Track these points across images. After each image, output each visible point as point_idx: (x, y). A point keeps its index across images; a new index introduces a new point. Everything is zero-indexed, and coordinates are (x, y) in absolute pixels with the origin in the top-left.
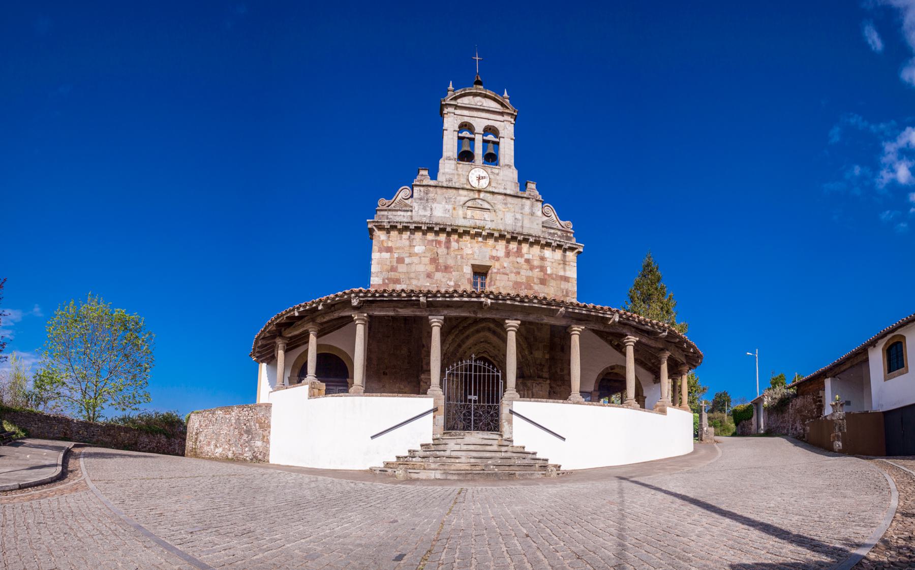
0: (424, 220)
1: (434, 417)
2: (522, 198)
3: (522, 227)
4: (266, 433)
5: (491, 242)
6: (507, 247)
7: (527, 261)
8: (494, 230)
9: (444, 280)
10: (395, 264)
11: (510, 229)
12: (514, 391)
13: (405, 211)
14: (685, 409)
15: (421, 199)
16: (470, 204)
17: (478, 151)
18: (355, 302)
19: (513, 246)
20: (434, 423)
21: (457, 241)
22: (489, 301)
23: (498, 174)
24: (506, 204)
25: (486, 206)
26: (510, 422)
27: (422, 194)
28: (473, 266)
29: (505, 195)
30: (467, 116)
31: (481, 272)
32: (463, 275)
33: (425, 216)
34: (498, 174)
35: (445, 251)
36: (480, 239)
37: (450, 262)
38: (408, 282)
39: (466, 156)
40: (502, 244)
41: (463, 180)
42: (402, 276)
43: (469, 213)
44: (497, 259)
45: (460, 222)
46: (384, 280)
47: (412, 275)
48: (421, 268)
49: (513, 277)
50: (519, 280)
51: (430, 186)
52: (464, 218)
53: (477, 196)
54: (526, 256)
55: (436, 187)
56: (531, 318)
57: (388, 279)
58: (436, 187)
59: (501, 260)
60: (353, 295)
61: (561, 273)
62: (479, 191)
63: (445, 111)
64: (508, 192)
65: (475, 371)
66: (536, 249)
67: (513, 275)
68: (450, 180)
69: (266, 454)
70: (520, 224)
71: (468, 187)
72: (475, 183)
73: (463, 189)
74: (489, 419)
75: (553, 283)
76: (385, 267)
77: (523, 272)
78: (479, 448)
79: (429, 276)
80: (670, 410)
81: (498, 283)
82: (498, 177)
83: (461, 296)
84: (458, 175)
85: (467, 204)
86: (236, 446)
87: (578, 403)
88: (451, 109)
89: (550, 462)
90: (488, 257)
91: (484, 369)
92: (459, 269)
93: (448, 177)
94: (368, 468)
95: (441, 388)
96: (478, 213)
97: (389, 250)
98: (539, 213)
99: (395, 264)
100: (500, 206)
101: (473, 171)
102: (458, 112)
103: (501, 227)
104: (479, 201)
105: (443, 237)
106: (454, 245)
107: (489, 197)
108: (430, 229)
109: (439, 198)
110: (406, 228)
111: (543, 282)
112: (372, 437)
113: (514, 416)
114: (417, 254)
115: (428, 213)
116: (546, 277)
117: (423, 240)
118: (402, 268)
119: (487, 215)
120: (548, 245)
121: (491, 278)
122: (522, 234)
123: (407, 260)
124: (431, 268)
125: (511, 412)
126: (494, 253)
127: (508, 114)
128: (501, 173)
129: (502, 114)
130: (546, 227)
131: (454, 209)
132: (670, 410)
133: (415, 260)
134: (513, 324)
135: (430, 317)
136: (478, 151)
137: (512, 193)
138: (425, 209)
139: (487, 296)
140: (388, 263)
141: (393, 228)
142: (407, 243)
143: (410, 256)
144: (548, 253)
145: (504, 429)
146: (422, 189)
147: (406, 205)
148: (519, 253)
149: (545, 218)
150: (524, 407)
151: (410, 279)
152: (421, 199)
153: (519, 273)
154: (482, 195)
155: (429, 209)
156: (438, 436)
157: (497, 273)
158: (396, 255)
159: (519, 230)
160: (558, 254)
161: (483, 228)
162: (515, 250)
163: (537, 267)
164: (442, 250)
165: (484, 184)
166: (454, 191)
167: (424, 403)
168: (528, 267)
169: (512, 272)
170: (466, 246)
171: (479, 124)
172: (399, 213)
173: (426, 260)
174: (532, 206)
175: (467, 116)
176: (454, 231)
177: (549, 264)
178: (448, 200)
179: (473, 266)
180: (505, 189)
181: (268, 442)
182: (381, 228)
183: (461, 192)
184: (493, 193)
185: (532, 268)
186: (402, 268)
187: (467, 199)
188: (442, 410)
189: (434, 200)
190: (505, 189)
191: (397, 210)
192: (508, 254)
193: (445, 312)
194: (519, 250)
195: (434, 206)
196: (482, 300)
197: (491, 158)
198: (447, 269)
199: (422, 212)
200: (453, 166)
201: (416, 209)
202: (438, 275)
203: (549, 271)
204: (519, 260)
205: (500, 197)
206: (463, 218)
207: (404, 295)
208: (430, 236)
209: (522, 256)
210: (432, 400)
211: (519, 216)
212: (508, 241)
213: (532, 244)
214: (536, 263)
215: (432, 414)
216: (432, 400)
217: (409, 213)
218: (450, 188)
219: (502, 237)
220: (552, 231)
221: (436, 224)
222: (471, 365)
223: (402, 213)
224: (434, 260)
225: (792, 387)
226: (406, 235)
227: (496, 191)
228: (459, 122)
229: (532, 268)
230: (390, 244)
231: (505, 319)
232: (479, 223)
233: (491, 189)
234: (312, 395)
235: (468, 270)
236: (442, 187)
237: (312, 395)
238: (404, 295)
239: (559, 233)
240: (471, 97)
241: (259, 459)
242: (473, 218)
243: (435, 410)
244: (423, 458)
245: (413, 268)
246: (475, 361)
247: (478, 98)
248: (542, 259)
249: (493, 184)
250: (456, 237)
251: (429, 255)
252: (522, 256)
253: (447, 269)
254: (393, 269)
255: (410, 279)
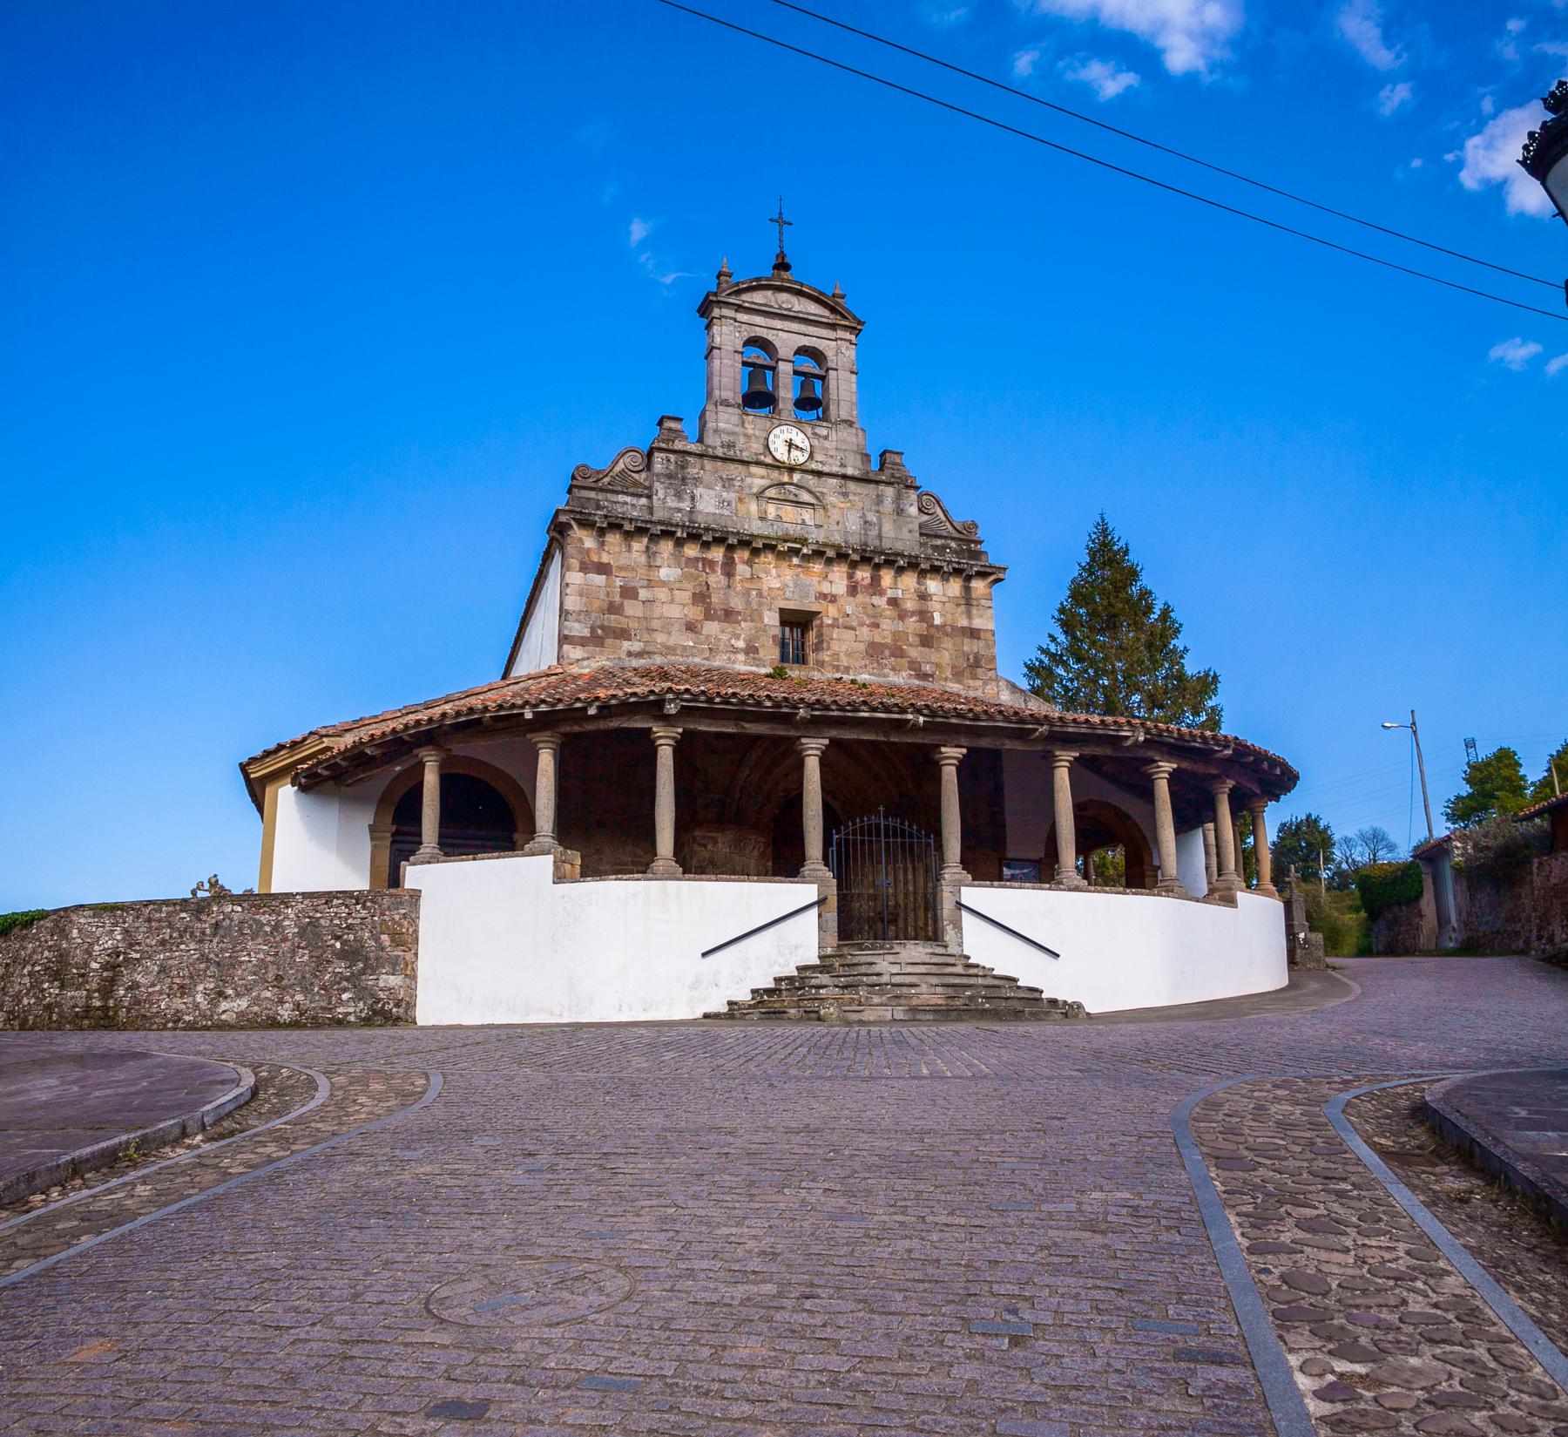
0: (678, 517)
1: (820, 916)
2: (878, 482)
3: (880, 537)
4: (409, 956)
5: (818, 567)
6: (850, 576)
7: (893, 602)
8: (826, 545)
9: (724, 637)
10: (617, 599)
11: (855, 540)
12: (959, 870)
13: (633, 495)
14: (1270, 895)
15: (669, 476)
16: (772, 493)
17: (787, 392)
18: (671, 709)
19: (863, 574)
20: (820, 928)
21: (749, 563)
22: (921, 719)
23: (826, 438)
24: (845, 495)
25: (806, 497)
26: (958, 926)
27: (672, 467)
28: (782, 611)
29: (845, 477)
30: (760, 326)
31: (798, 622)
32: (765, 628)
33: (679, 510)
34: (826, 438)
35: (723, 580)
36: (795, 561)
37: (737, 603)
38: (646, 637)
39: (759, 399)
40: (839, 573)
41: (757, 447)
42: (633, 625)
43: (772, 510)
44: (833, 599)
45: (756, 527)
46: (593, 629)
47: (655, 624)
48: (674, 612)
49: (865, 632)
50: (878, 639)
51: (690, 454)
52: (762, 519)
53: (786, 479)
54: (890, 593)
55: (701, 456)
56: (985, 743)
57: (602, 627)
58: (701, 456)
59: (841, 601)
60: (670, 696)
61: (964, 622)
62: (791, 469)
63: (716, 312)
64: (850, 471)
65: (887, 836)
66: (909, 580)
67: (865, 630)
68: (731, 445)
69: (411, 1006)
70: (874, 533)
71: (769, 460)
72: (781, 453)
73: (758, 463)
74: (925, 920)
75: (947, 643)
76: (597, 604)
77: (886, 625)
78: (934, 969)
79: (691, 627)
80: (1242, 897)
81: (835, 646)
82: (827, 444)
83: (874, 710)
84: (746, 435)
85: (768, 493)
86: (306, 991)
87: (1077, 889)
88: (726, 312)
89: (1044, 996)
90: (812, 594)
91: (903, 831)
92: (755, 616)
93: (726, 438)
94: (699, 1014)
95: (826, 865)
96: (789, 512)
97: (603, 569)
98: (913, 510)
99: (617, 599)
100: (832, 499)
101: (777, 431)
102: (742, 317)
103: (837, 539)
104: (792, 488)
105: (717, 554)
106: (742, 570)
107: (811, 481)
108: (694, 537)
109: (707, 477)
110: (641, 531)
111: (926, 641)
112: (704, 955)
113: (964, 914)
114: (664, 584)
115: (686, 505)
116: (932, 631)
117: (677, 556)
118: (632, 609)
119: (807, 515)
120: (935, 570)
121: (820, 636)
122: (882, 553)
123: (643, 594)
124: (694, 613)
125: (960, 906)
126: (826, 588)
127: (845, 328)
128: (833, 436)
129: (833, 327)
130: (927, 535)
131: (740, 500)
132: (1242, 897)
133: (662, 594)
134: (952, 753)
135: (804, 741)
136: (787, 392)
137: (856, 473)
138: (679, 496)
139: (919, 711)
140: (602, 596)
141: (615, 526)
142: (643, 559)
143: (648, 587)
144: (933, 585)
145: (947, 938)
146: (672, 457)
147: (636, 484)
148: (875, 586)
149: (925, 518)
150: (977, 896)
151: (651, 630)
152: (669, 476)
153: (877, 626)
154: (796, 477)
155: (687, 497)
156: (829, 951)
157: (832, 626)
158: (618, 583)
159: (873, 543)
160: (955, 587)
161: (804, 541)
162: (868, 581)
163: (913, 613)
164: (717, 579)
165: (799, 457)
166: (740, 467)
167: (805, 892)
168: (895, 614)
169: (862, 624)
170: (767, 572)
171: (787, 340)
172: (621, 498)
173: (685, 596)
174: (898, 498)
175: (760, 326)
176: (745, 542)
177: (938, 606)
178: (727, 483)
179: (782, 611)
180: (842, 465)
181: (414, 978)
182: (586, 524)
183: (754, 469)
184: (819, 474)
185: (902, 616)
186: (632, 609)
187: (765, 482)
188: (833, 901)
189: (697, 481)
190: (842, 465)
191: (617, 492)
192: (853, 590)
193: (834, 733)
194: (876, 580)
195: (697, 492)
196: (910, 717)
197: (811, 403)
198: (729, 615)
199: (672, 502)
200: (735, 419)
201: (661, 494)
202: (712, 628)
203: (938, 620)
204: (876, 600)
205: (834, 481)
206: (752, 519)
207: (768, 704)
208: (691, 551)
209: (882, 593)
210: (815, 887)
211: (872, 517)
212: (854, 565)
213: (900, 571)
214: (910, 605)
215: (815, 911)
216: (815, 887)
217: (644, 501)
218: (732, 460)
219: (842, 556)
220: (939, 542)
221: (707, 529)
222: (878, 826)
223: (628, 499)
224: (701, 598)
225: (1539, 814)
226: (639, 545)
227: (826, 469)
228: (745, 336)
229: (902, 616)
230: (605, 559)
231: (939, 746)
232: (794, 531)
233: (814, 466)
234: (559, 878)
235: (771, 619)
236: (715, 457)
237: (559, 878)
238: (768, 704)
239: (953, 545)
240: (769, 293)
241: (390, 1014)
242: (779, 518)
243: (821, 902)
244: (845, 987)
245: (657, 610)
246: (886, 817)
247: (784, 296)
248: (923, 596)
249: (818, 457)
250: (746, 554)
251: (690, 586)
252: (882, 593)
253: (729, 615)
254: (613, 609)
255: (651, 630)
